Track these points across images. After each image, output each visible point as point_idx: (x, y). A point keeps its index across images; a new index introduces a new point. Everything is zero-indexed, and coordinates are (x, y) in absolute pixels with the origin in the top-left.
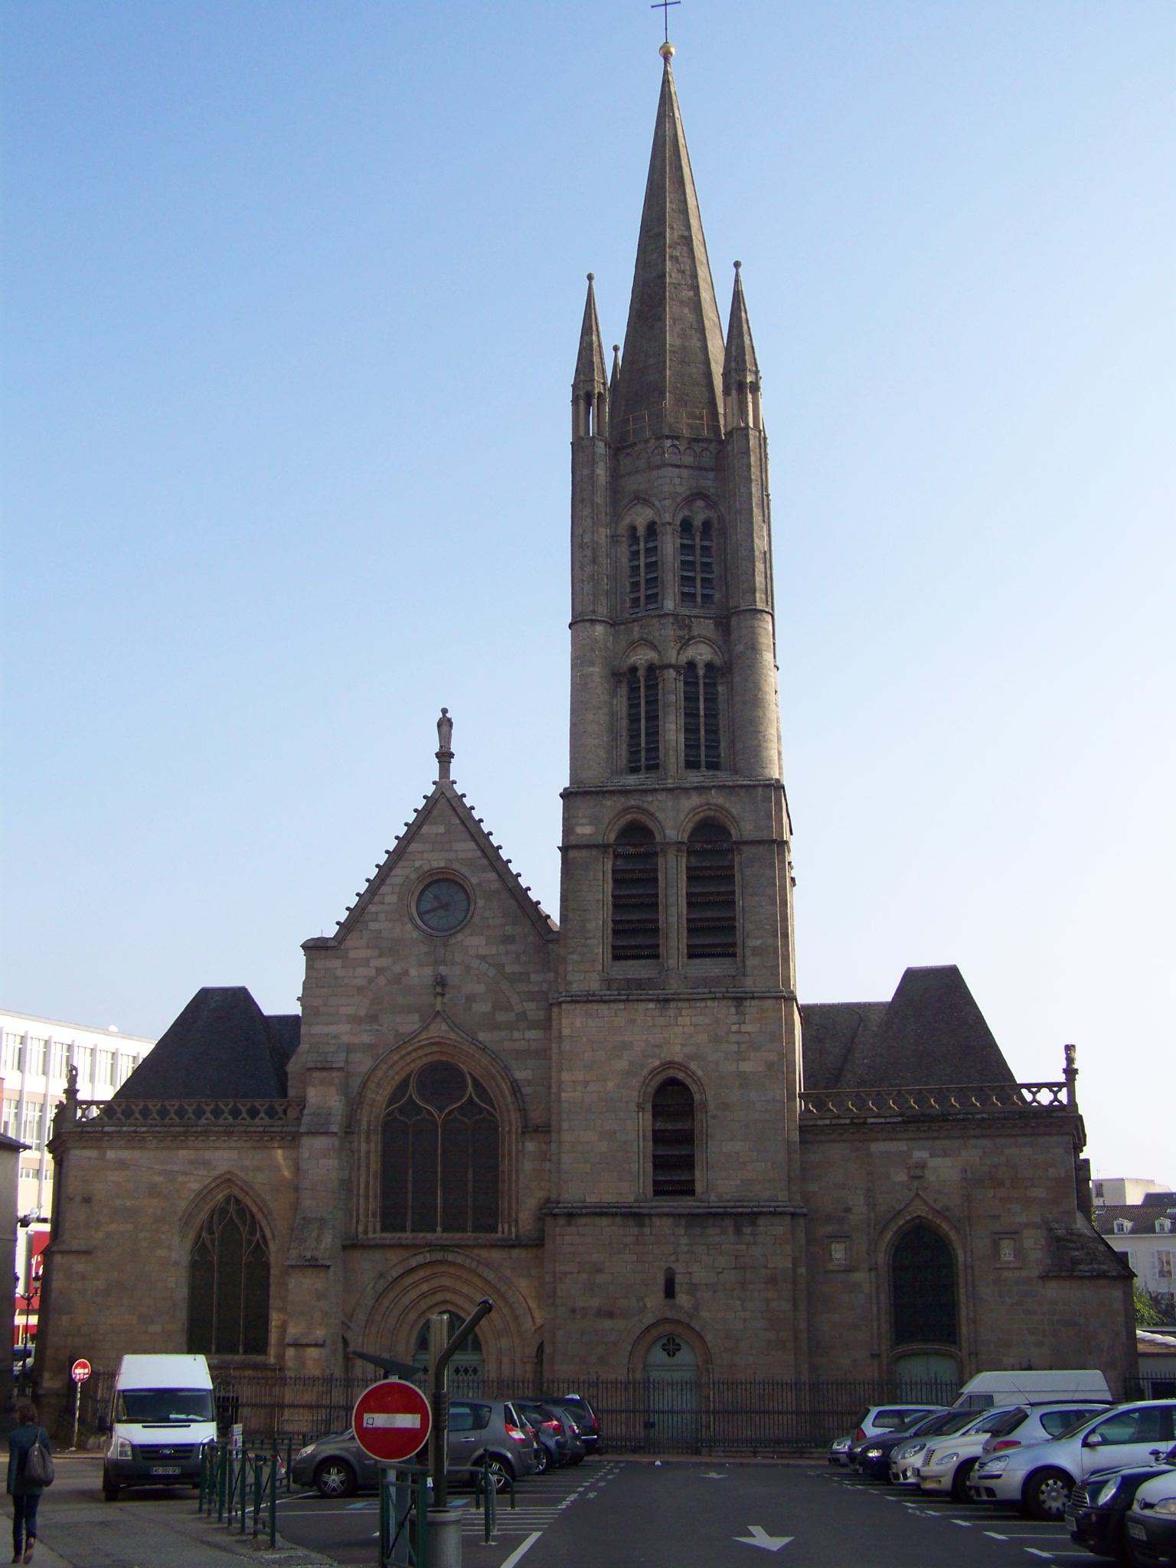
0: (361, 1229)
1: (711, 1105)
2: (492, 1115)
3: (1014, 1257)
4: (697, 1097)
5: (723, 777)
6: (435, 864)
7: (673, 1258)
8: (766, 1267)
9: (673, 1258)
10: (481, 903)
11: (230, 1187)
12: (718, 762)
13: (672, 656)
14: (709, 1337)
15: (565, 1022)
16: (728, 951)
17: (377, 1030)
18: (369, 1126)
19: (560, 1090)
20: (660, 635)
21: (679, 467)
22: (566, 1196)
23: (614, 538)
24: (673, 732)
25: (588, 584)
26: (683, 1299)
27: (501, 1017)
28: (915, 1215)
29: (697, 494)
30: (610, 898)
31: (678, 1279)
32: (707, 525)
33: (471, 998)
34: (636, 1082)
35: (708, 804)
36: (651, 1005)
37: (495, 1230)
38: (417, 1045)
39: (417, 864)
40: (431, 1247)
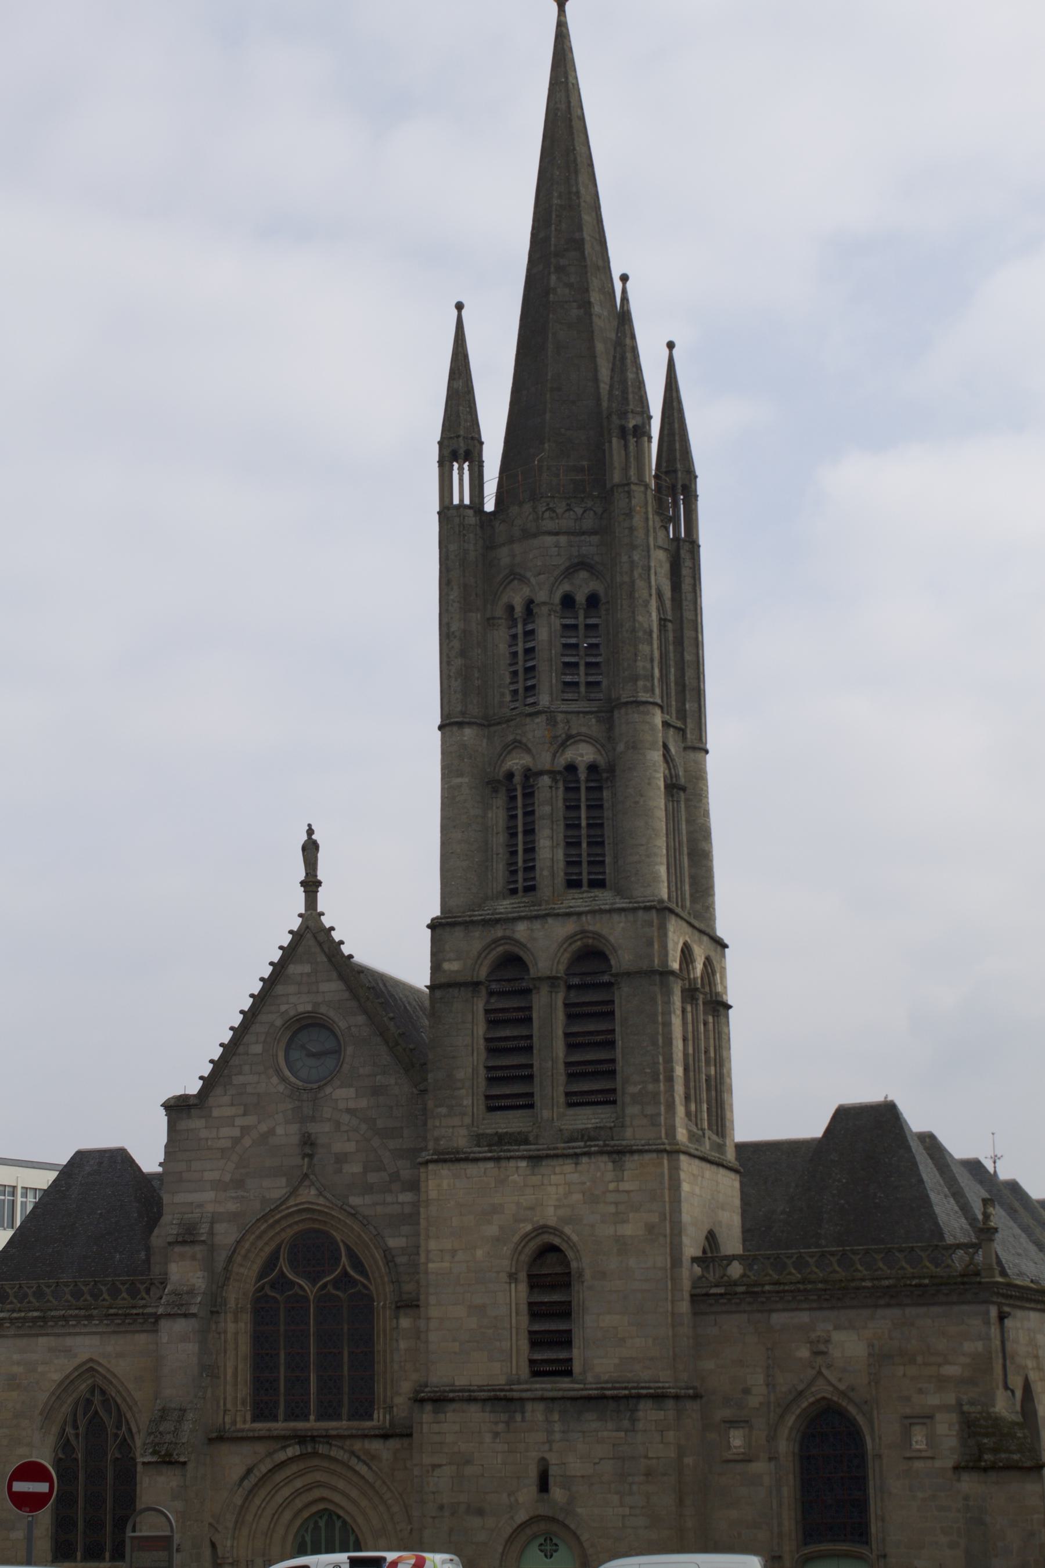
0: (228, 1419)
1: (588, 1274)
2: (365, 1286)
3: (926, 1445)
4: (574, 1265)
5: (605, 898)
6: (301, 1009)
8: (646, 1457)
9: (546, 1447)
10: (350, 1050)
11: (94, 1376)
13: (544, 760)
14: (583, 1538)
16: (608, 1099)
17: (243, 1197)
18: (237, 1304)
19: (428, 1260)
20: (534, 737)
21: (557, 534)
22: (434, 1380)
23: (490, 622)
25: (456, 680)
26: (557, 1493)
27: (373, 1178)
28: (819, 1396)
30: (482, 1042)
31: (553, 1471)
32: (593, 601)
33: (341, 1159)
34: (506, 1250)
35: (583, 932)
36: (523, 1164)
37: (370, 1418)
38: (286, 1212)
39: (283, 1008)
40: (301, 1439)
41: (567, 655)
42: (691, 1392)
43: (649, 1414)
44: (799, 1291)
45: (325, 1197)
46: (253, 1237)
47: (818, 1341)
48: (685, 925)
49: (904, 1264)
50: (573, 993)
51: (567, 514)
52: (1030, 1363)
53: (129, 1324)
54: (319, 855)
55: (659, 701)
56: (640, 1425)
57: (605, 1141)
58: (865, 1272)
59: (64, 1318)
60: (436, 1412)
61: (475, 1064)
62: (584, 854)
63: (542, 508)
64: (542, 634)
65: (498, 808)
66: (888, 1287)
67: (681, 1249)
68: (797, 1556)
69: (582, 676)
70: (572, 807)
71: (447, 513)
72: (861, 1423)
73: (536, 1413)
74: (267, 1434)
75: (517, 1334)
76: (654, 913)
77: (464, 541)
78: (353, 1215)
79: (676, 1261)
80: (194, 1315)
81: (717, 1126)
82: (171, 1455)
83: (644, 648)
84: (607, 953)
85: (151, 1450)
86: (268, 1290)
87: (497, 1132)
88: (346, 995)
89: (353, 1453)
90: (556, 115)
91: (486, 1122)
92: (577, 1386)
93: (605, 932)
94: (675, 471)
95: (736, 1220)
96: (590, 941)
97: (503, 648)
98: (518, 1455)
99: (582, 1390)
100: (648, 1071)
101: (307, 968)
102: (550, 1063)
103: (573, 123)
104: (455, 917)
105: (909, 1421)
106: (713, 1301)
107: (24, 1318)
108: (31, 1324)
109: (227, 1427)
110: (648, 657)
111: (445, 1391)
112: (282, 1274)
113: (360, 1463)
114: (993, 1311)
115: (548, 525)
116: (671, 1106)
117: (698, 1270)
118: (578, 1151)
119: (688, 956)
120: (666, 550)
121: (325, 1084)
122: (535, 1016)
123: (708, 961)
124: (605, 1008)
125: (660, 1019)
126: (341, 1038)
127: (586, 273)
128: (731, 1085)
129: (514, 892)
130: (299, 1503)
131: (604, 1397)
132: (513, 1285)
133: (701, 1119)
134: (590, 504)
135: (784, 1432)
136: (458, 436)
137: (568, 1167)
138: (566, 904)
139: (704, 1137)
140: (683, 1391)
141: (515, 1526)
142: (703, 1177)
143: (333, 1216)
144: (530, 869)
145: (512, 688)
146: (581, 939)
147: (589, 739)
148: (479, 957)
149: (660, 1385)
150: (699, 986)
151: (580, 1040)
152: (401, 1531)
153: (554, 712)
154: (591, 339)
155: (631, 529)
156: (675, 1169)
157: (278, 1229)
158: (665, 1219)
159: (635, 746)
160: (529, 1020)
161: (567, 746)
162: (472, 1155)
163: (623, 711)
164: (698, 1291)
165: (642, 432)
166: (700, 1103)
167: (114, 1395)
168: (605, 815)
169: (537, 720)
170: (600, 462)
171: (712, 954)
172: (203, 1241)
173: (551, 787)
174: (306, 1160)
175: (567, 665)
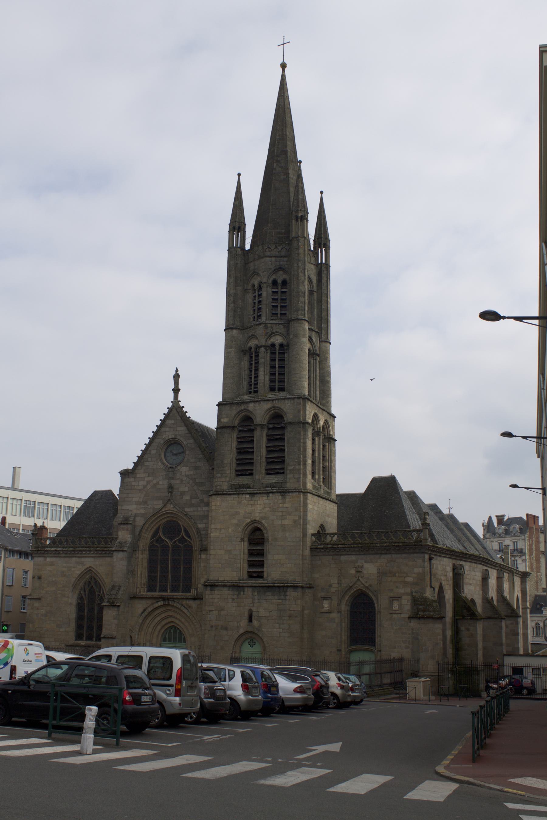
0: (138, 590)
1: (270, 539)
2: (190, 542)
4: (266, 535)
5: (283, 394)
6: (170, 437)
7: (252, 605)
9: (252, 605)
10: (187, 452)
12: (284, 388)
13: (263, 342)
14: (265, 640)
15: (213, 503)
16: (281, 472)
17: (146, 508)
20: (259, 333)
21: (271, 257)
22: (211, 578)
23: (246, 291)
24: (264, 376)
26: (255, 623)
27: (194, 501)
28: (358, 588)
29: (279, 268)
30: (235, 449)
31: (254, 614)
32: (284, 283)
33: (182, 494)
34: (240, 529)
35: (274, 407)
36: (248, 496)
37: (190, 592)
38: (162, 513)
39: (164, 437)
40: (164, 599)
41: (274, 303)
42: (308, 585)
43: (291, 593)
44: (352, 547)
45: (176, 508)
46: (150, 522)
47: (358, 567)
48: (315, 406)
49: (392, 537)
50: (270, 431)
51: (275, 249)
52: (443, 578)
53: (104, 554)
54: (180, 379)
55: (307, 319)
56: (288, 598)
57: (279, 488)
58: (377, 541)
59: (81, 551)
60: (211, 590)
61: (232, 457)
62: (277, 378)
63: (266, 247)
64: (264, 294)
65: (245, 361)
66: (386, 546)
67: (307, 530)
68: (347, 650)
69: (279, 311)
70: (273, 360)
71: (231, 251)
72: (374, 599)
73: (248, 592)
74: (151, 596)
75: (243, 561)
76: (301, 400)
77: (236, 260)
78: (186, 515)
79: (305, 535)
80: (126, 551)
81: (328, 485)
82: (114, 603)
83: (302, 299)
84: (283, 415)
85: (107, 601)
86: (155, 543)
87: (238, 484)
88: (187, 432)
89: (182, 605)
90: (280, 107)
91: (235, 480)
92: (264, 582)
93: (282, 407)
94: (321, 238)
95: (335, 522)
96: (277, 411)
97: (250, 301)
98: (241, 608)
99: (266, 583)
100: (296, 461)
101: (173, 422)
102: (260, 457)
103: (286, 110)
104: (226, 402)
105: (392, 599)
106: (319, 551)
107: (67, 550)
108: (69, 553)
109: (137, 593)
110: (303, 302)
111: (215, 582)
112: (160, 537)
113: (185, 609)
114: (427, 557)
115: (268, 253)
116: (305, 475)
117: (314, 539)
118: (268, 491)
119: (317, 418)
120: (314, 265)
121: (178, 466)
122: (255, 439)
123: (326, 422)
124: (282, 437)
125: (302, 441)
126: (184, 448)
127: (288, 163)
128: (335, 470)
129: (250, 393)
130: (163, 623)
131: (274, 586)
132: (242, 543)
133: (320, 482)
134: (284, 246)
135: (344, 602)
136: (236, 221)
137: (265, 498)
138: (268, 396)
139: (321, 488)
140: (305, 585)
141: (239, 634)
142: (319, 503)
143: (179, 516)
144: (256, 384)
145: (253, 316)
146: (273, 410)
147: (280, 334)
148: (235, 417)
149: (296, 582)
150: (321, 430)
151: (272, 449)
152: (199, 635)
153: (266, 323)
154: (288, 187)
155: (298, 254)
156: (305, 499)
157: (159, 520)
158: (301, 518)
159: (296, 336)
160: (253, 441)
161: (272, 337)
162: (229, 492)
163: (293, 322)
164: (314, 547)
165: (304, 218)
166: (320, 475)
167: (98, 580)
168: (285, 363)
169: (260, 327)
170: (288, 232)
171: (328, 419)
172: (131, 524)
173: (265, 352)
174: (170, 494)
175: (273, 306)
